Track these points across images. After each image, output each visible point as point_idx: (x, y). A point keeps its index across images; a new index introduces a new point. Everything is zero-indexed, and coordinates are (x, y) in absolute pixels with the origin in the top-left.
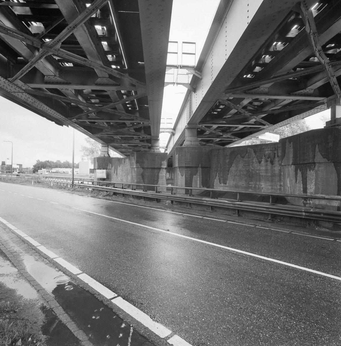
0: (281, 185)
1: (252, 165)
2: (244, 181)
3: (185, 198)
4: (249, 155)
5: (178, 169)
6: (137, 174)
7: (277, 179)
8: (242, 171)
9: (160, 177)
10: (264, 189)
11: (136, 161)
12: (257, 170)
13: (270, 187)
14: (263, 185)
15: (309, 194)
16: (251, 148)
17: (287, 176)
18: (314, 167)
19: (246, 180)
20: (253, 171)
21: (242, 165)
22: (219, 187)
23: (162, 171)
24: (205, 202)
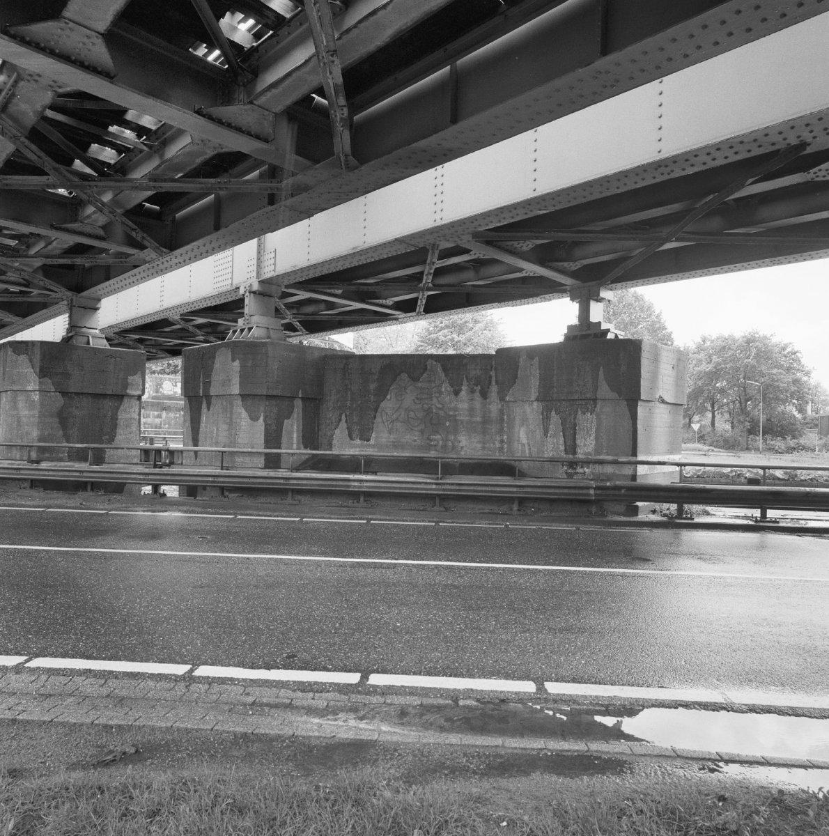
0: (502, 441)
1: (437, 398)
2: (417, 433)
3: (286, 479)
4: (430, 377)
5: (239, 402)
6: (40, 412)
7: (494, 428)
8: (413, 411)
9: (121, 423)
10: (465, 449)
11: (41, 370)
12: (450, 409)
13: (479, 446)
14: (463, 440)
15: (580, 456)
16: (436, 361)
17: (517, 422)
18: (595, 407)
19: (422, 432)
20: (440, 412)
21: (413, 398)
22: (344, 446)
23: (126, 405)
24: (356, 484)
